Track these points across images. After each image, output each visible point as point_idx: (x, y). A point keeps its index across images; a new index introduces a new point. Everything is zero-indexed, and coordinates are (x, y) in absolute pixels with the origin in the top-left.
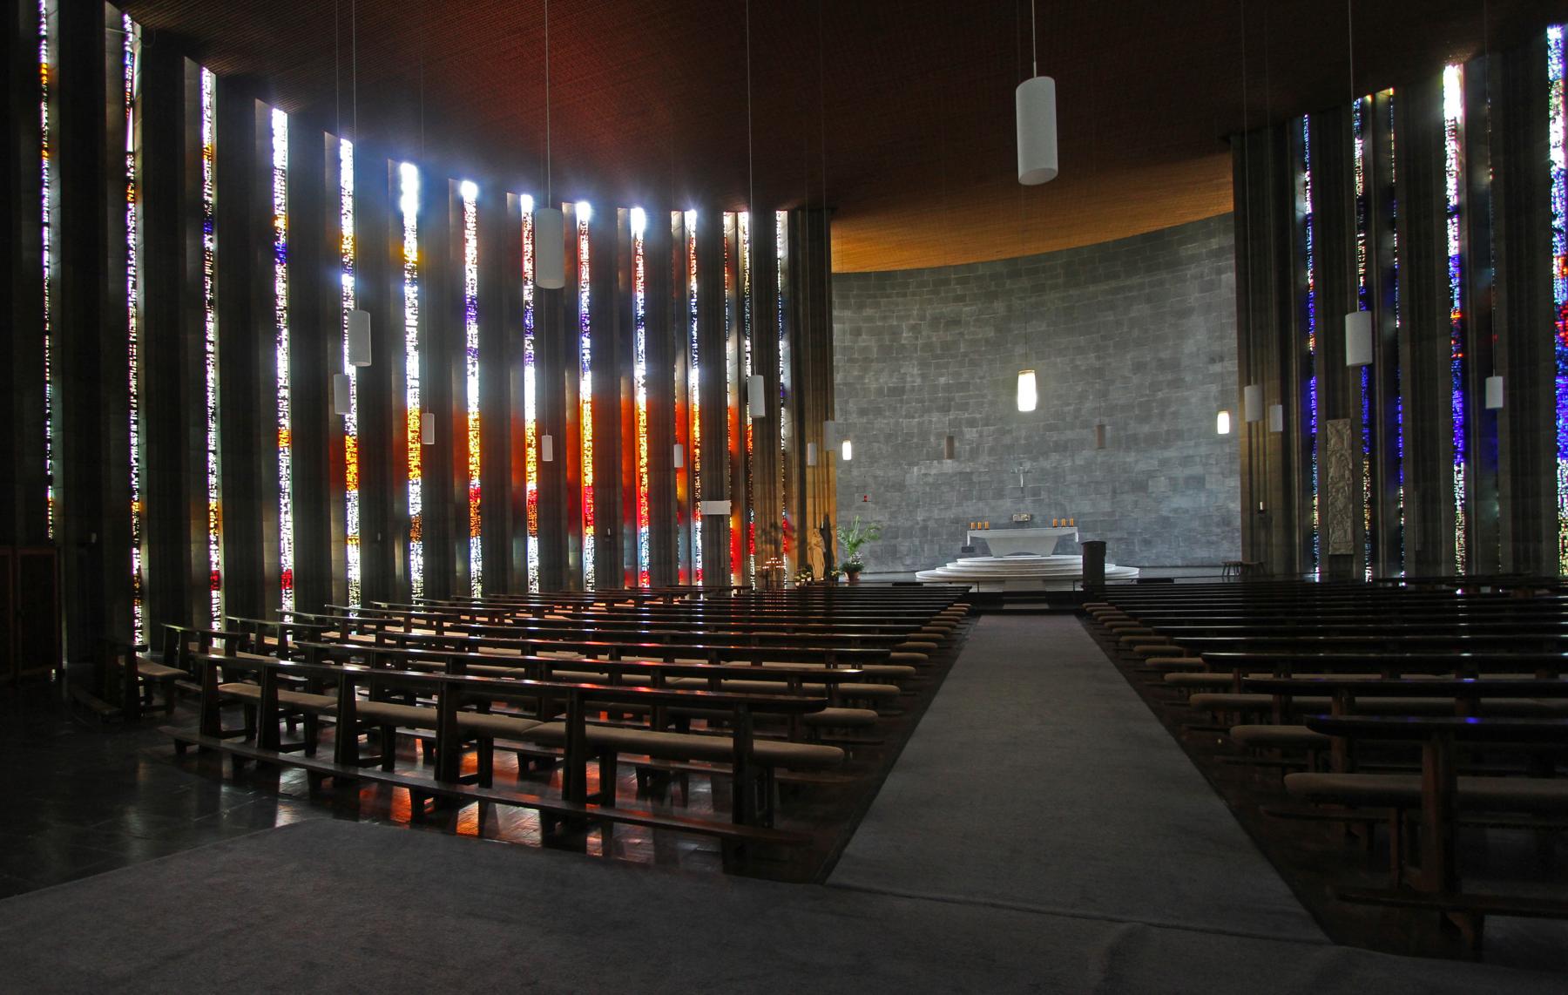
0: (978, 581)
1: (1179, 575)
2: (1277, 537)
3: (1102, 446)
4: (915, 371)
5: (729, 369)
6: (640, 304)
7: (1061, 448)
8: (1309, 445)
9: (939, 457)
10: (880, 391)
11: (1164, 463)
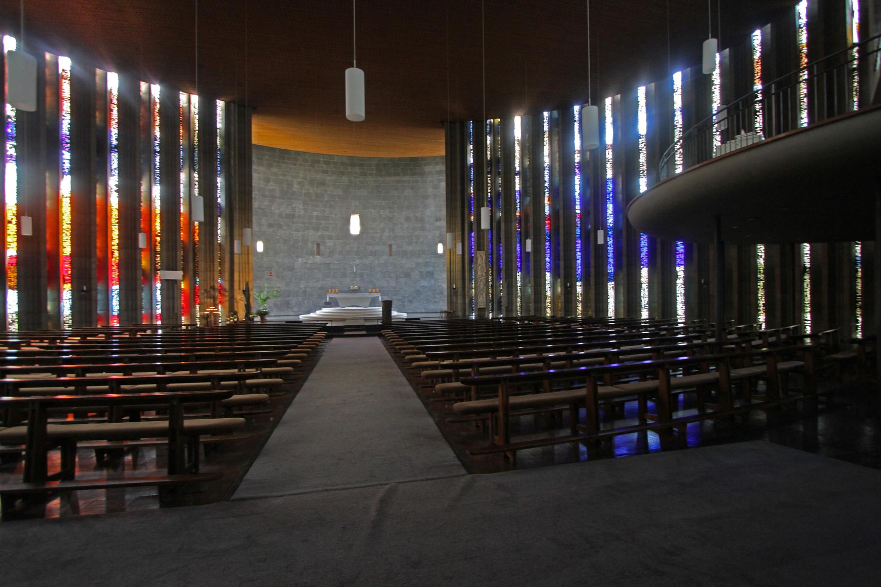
1: (423, 317)
2: (460, 301)
3: (390, 255)
4: (301, 207)
5: (182, 188)
7: (374, 254)
9: (312, 254)
10: (280, 215)
11: (418, 264)
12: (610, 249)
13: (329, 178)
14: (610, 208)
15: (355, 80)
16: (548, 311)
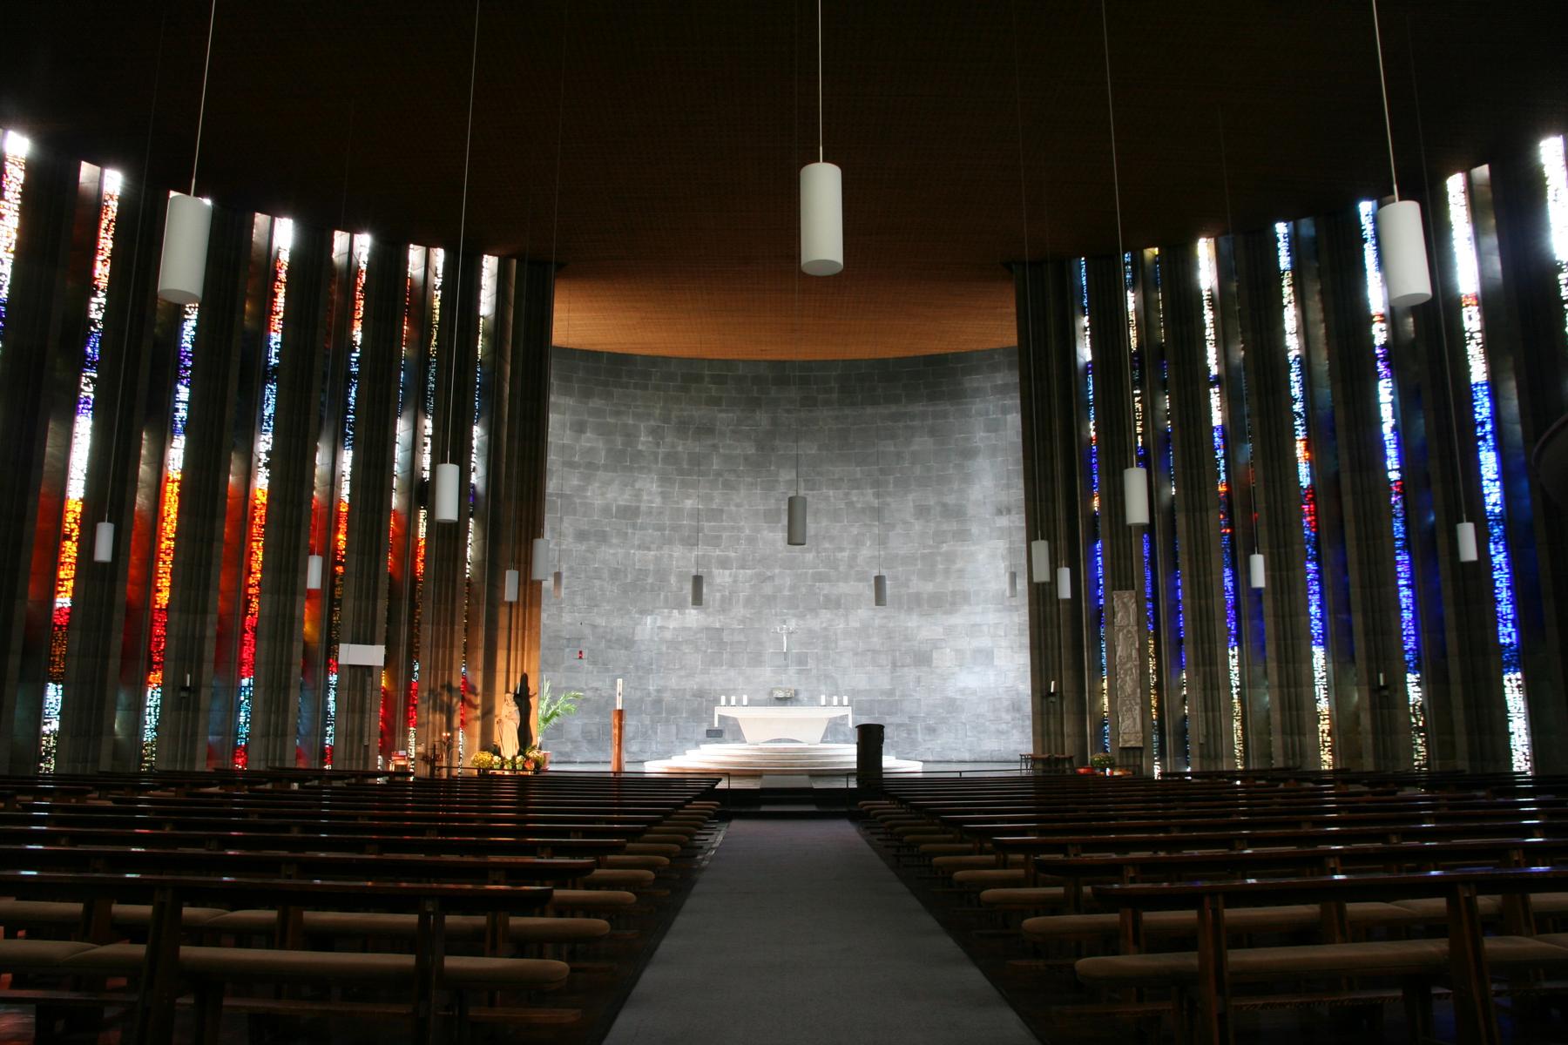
0: (728, 774)
4: (655, 488)
6: (274, 349)
7: (834, 603)
8: (1098, 617)
9: (680, 606)
10: (606, 510)
12: (1501, 578)
13: (723, 417)
14: (1489, 462)
15: (823, 189)
16: (1326, 757)
